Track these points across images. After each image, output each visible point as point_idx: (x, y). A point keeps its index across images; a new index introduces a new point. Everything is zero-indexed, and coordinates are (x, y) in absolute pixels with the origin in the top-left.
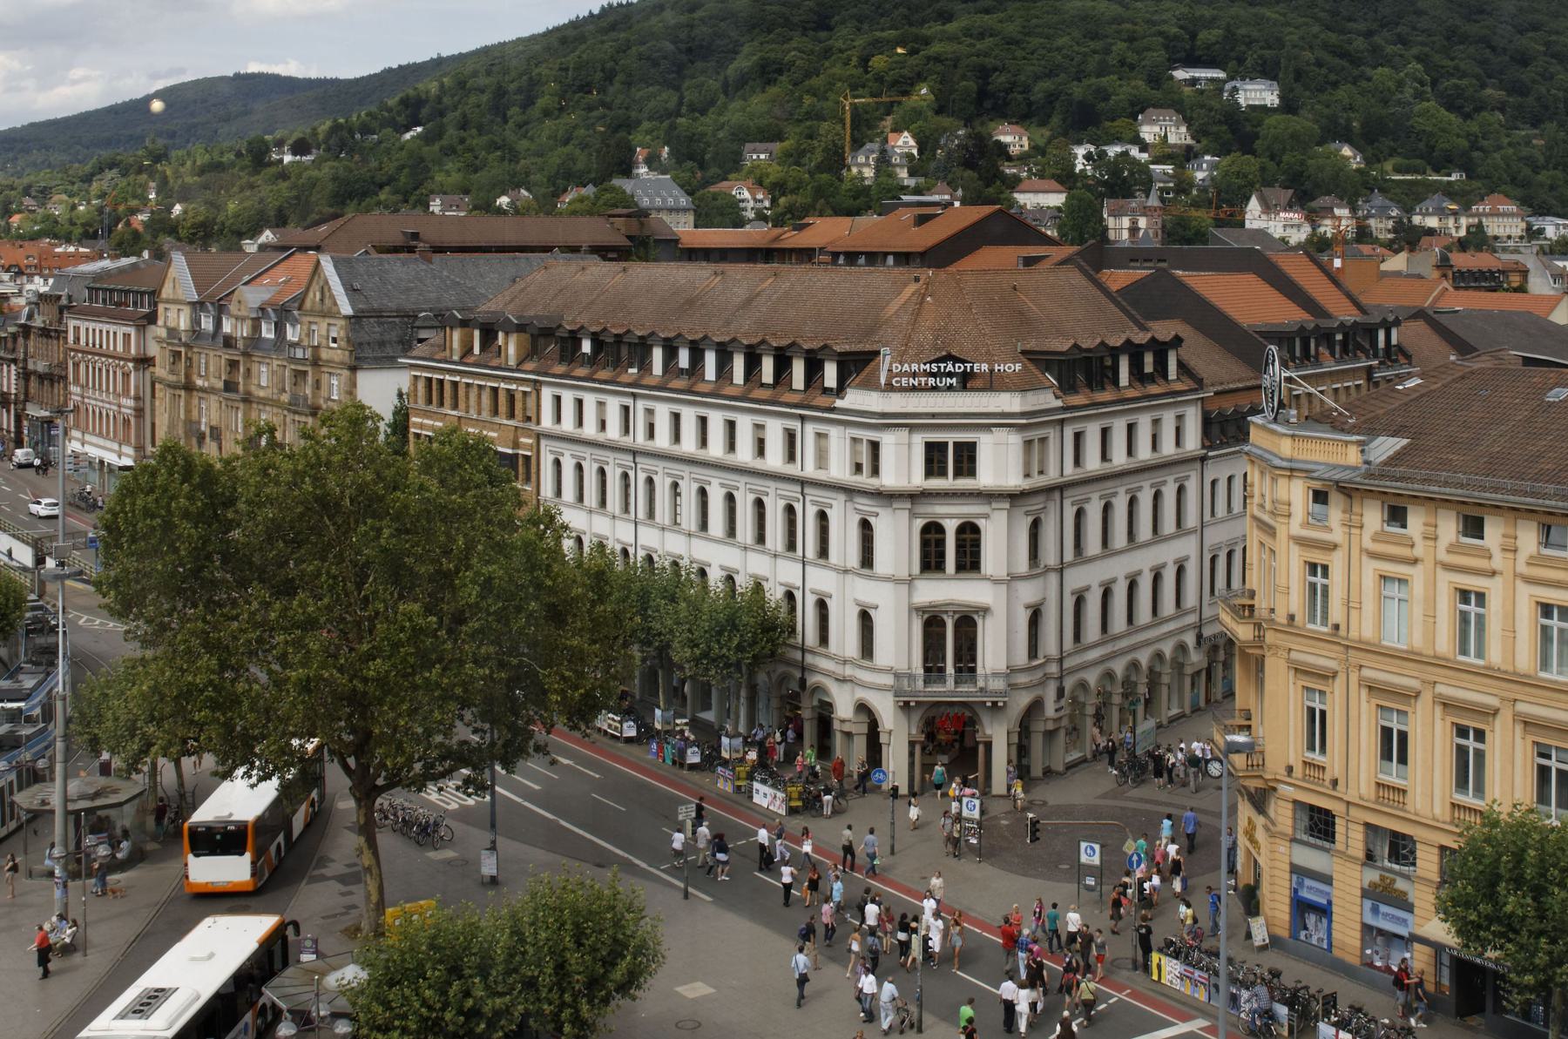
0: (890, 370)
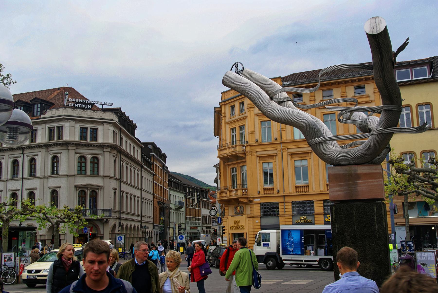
0: (68, 101)
